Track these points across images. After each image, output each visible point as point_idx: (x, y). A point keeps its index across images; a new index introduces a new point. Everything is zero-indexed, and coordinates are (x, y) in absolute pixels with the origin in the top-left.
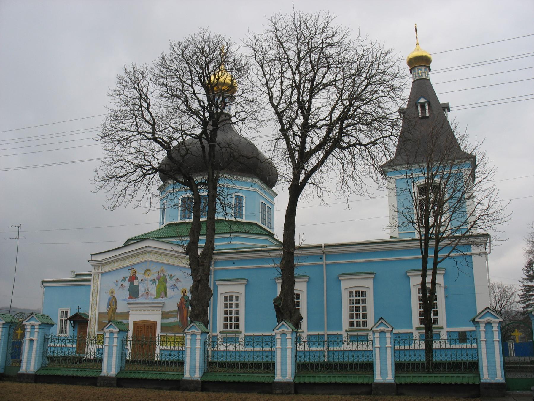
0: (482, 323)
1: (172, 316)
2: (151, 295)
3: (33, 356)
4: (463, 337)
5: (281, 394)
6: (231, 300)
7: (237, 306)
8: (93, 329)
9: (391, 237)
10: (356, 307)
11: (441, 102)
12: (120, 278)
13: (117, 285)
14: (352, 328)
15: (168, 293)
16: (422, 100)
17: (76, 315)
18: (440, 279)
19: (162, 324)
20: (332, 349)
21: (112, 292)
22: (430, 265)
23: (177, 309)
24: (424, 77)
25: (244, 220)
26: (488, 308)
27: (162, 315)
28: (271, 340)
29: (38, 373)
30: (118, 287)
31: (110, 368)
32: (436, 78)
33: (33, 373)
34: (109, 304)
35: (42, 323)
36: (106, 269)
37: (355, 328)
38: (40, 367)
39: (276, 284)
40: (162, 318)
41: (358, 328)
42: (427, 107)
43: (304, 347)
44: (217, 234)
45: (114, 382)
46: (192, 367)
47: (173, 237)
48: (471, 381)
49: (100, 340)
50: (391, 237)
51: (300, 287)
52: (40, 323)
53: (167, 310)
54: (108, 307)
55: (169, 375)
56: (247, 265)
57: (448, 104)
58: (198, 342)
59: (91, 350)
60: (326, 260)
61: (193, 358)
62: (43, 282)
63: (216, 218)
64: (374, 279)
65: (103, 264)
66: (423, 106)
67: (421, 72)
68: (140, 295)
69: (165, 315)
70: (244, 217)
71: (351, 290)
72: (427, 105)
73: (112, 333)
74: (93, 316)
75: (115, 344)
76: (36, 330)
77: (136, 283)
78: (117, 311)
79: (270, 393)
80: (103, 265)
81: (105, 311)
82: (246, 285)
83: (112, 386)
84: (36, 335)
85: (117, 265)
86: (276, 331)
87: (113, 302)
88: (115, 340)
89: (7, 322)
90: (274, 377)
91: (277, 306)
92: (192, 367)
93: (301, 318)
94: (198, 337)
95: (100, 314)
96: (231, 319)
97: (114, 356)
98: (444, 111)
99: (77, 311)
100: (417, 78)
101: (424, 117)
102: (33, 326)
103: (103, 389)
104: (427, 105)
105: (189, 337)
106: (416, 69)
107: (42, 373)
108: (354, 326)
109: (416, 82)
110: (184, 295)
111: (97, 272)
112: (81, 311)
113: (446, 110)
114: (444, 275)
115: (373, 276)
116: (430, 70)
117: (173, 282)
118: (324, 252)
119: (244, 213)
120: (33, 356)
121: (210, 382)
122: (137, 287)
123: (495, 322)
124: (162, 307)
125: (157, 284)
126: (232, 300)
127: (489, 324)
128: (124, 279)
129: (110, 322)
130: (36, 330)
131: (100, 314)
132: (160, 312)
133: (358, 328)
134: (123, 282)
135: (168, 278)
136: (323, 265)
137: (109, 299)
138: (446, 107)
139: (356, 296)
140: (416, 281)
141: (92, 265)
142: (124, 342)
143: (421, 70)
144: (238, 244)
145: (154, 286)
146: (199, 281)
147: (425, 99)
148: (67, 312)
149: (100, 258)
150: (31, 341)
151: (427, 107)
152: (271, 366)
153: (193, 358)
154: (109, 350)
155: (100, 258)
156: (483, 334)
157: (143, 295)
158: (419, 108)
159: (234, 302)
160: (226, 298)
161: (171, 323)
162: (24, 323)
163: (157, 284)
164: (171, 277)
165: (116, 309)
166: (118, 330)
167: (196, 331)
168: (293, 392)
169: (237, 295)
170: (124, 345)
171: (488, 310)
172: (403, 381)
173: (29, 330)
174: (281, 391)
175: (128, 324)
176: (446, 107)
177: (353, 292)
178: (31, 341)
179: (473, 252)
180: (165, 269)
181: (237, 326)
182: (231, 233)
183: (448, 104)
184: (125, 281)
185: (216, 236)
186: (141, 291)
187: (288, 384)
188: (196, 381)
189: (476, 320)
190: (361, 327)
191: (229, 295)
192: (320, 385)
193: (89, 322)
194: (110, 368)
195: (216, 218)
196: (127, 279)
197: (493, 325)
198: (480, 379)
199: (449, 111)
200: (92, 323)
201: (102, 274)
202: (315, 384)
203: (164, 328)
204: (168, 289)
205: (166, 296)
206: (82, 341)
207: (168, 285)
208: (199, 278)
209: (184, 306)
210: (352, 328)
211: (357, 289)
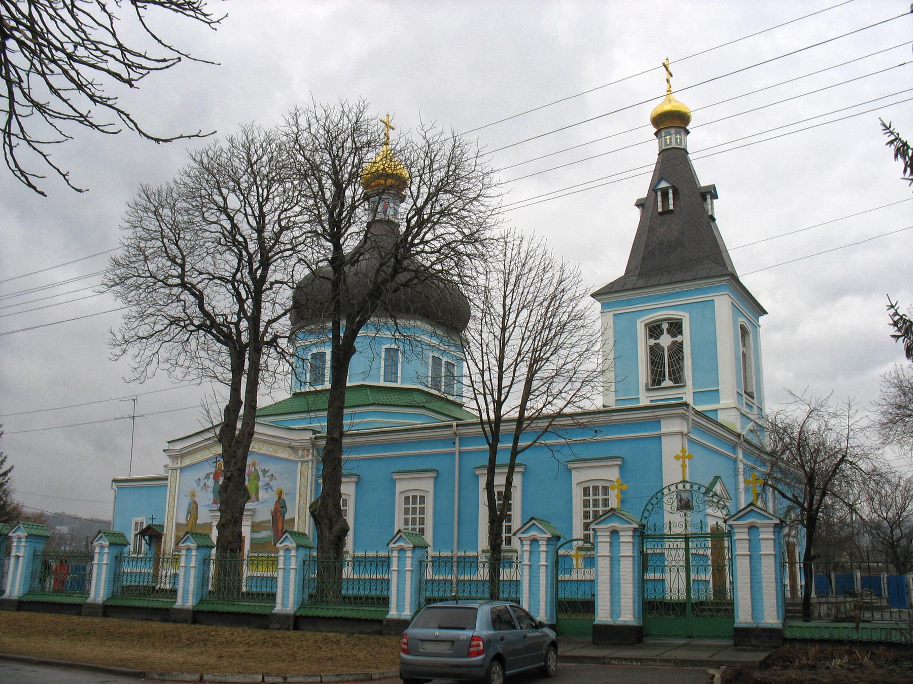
1: (264, 529)
3: (18, 577)
5: (278, 629)
6: (415, 501)
7: (422, 510)
8: (169, 543)
9: (604, 406)
12: (202, 475)
13: (199, 485)
15: (260, 495)
16: (663, 185)
17: (149, 528)
18: (517, 480)
19: (252, 539)
20: (703, 578)
21: (193, 495)
22: (503, 458)
23: (270, 518)
25: (399, 385)
27: (252, 526)
28: (385, 562)
29: (297, 615)
30: (200, 488)
31: (287, 601)
33: (16, 598)
34: (189, 512)
35: (29, 535)
36: (187, 461)
38: (27, 591)
39: (477, 476)
42: (671, 196)
43: (429, 574)
44: (347, 407)
45: (100, 611)
46: (185, 592)
47: (296, 413)
49: (176, 559)
50: (604, 406)
51: (347, 489)
53: (258, 519)
55: (160, 603)
56: (636, 432)
58: (409, 562)
59: (167, 571)
60: (460, 446)
61: (401, 591)
62: (115, 481)
63: (348, 385)
64: (621, 467)
65: (182, 455)
67: (672, 139)
70: (399, 380)
72: (670, 191)
73: (189, 549)
74: (170, 528)
75: (193, 564)
76: (23, 544)
78: (198, 522)
79: (266, 628)
80: (183, 456)
82: (357, 483)
83: (97, 615)
84: (22, 549)
85: (199, 457)
86: (391, 545)
88: (293, 560)
89: (29, 535)
92: (185, 592)
93: (345, 531)
94: (409, 554)
95: (178, 525)
97: (103, 577)
98: (704, 199)
100: (664, 148)
101: (666, 212)
103: (88, 619)
104: (670, 191)
105: (281, 553)
107: (205, 607)
110: (280, 498)
111: (175, 466)
112: (155, 522)
113: (709, 197)
114: (523, 474)
115: (620, 463)
117: (267, 479)
118: (455, 433)
119: (399, 375)
120: (18, 577)
121: (203, 612)
124: (253, 516)
126: (414, 502)
128: (207, 476)
129: (187, 533)
130: (23, 544)
131: (178, 525)
132: (250, 523)
134: (206, 481)
135: (260, 474)
136: (454, 453)
137: (189, 505)
140: (483, 482)
141: (170, 456)
142: (205, 562)
144: (374, 422)
147: (668, 182)
149: (179, 446)
150: (18, 557)
151: (671, 196)
152: (272, 597)
153: (401, 591)
155: (179, 446)
156: (526, 555)
158: (659, 198)
159: (601, 497)
160: (586, 491)
161: (262, 538)
162: (10, 534)
164: (265, 472)
165: (196, 518)
166: (294, 545)
168: (291, 628)
170: (423, 569)
173: (15, 544)
174: (278, 626)
176: (711, 193)
178: (18, 557)
179: (664, 430)
180: (257, 462)
182: (309, 412)
183: (714, 187)
185: (346, 411)
187: (286, 617)
188: (187, 611)
191: (591, 485)
192: (324, 618)
194: (287, 601)
195: (348, 385)
196: (211, 476)
197: (540, 542)
200: (168, 538)
201: (181, 469)
202: (318, 617)
203: (254, 544)
205: (258, 500)
206: (157, 560)
207: (261, 484)
209: (279, 514)
211: (414, 494)
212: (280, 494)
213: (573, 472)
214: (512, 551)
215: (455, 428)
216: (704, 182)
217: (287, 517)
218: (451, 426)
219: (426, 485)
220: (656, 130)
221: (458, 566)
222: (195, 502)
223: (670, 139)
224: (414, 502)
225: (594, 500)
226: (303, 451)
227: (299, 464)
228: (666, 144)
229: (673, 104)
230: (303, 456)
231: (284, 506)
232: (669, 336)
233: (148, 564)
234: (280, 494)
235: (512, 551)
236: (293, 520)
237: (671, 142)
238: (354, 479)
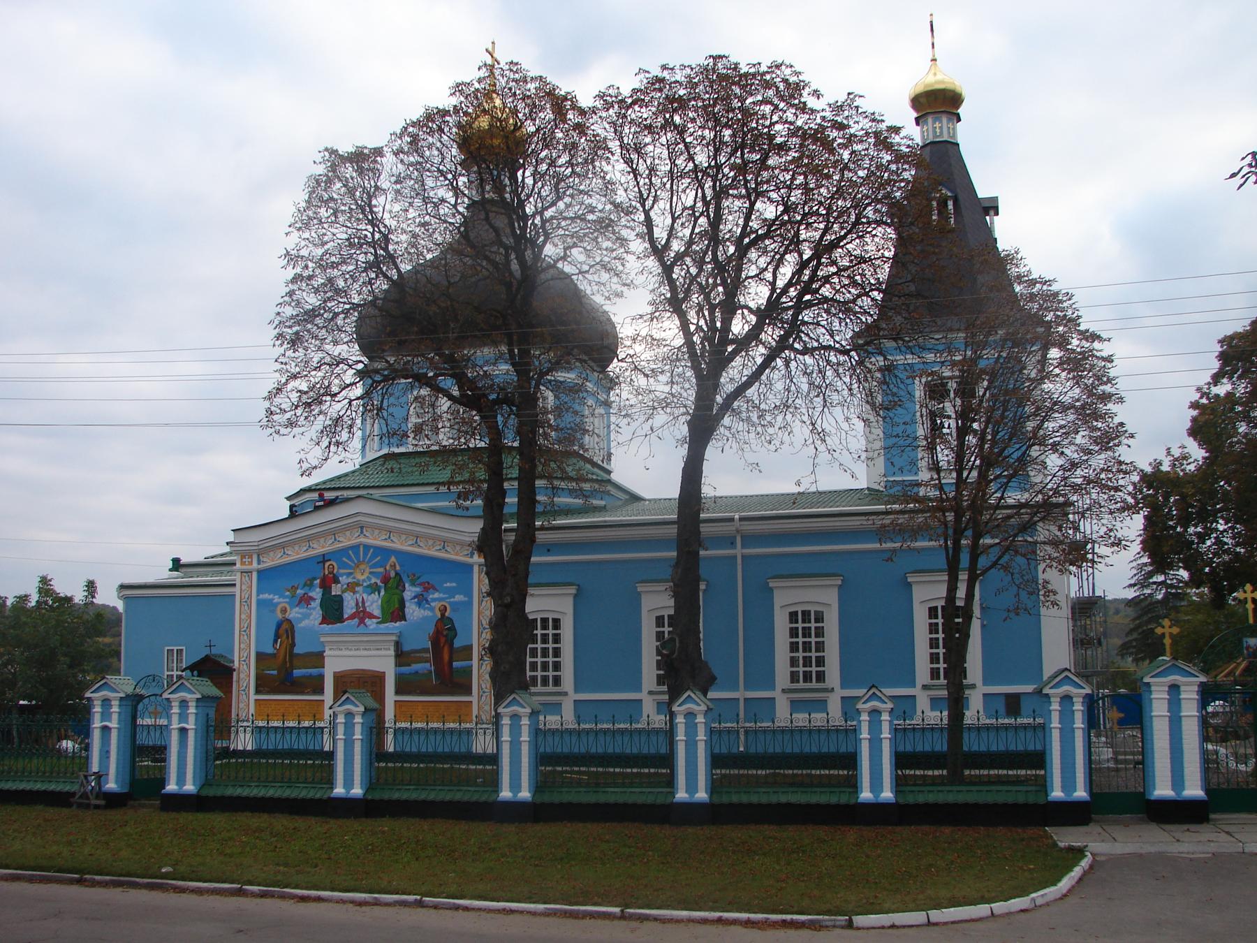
0: (1055, 695)
2: (371, 616)
4: (1013, 704)
11: (981, 194)
14: (795, 686)
24: (945, 138)
26: (1066, 669)
32: (971, 136)
35: (203, 697)
37: (801, 685)
40: (399, 664)
41: (808, 685)
48: (1031, 799)
52: (199, 696)
54: (275, 641)
57: (995, 199)
60: (743, 547)
62: (123, 587)
66: (943, 204)
67: (938, 128)
68: (346, 616)
69: (402, 657)
71: (793, 609)
77: (336, 590)
81: (269, 650)
87: (285, 630)
90: (673, 794)
91: (667, 656)
95: (260, 657)
96: (545, 667)
99: (206, 652)
102: (184, 704)
106: (930, 120)
108: (798, 681)
109: (928, 148)
110: (443, 615)
116: (959, 120)
122: (339, 600)
123: (1078, 695)
125: (382, 593)
126: (545, 627)
127: (1067, 698)
133: (808, 685)
138: (991, 207)
139: (804, 621)
143: (941, 122)
145: (375, 596)
146: (508, 606)
148: (180, 652)
150: (183, 731)
154: (345, 747)
157: (352, 617)
159: (551, 632)
160: (793, 617)
163: (382, 593)
165: (293, 645)
166: (362, 709)
167: (521, 710)
169: (556, 616)
171: (1066, 673)
172: (911, 799)
175: (322, 677)
176: (991, 207)
177: (796, 613)
181: (557, 681)
183: (995, 199)
186: (349, 608)
189: (1045, 691)
190: (814, 685)
191: (799, 609)
193: (235, 674)
198: (1047, 795)
199: (997, 214)
200: (242, 676)
204: (407, 604)
208: (508, 600)
209: (443, 640)
210: (795, 686)
211: (806, 608)
213: (914, 588)
214: (560, 694)
215: (737, 523)
216: (982, 192)
217: (458, 643)
218: (732, 520)
219: (825, 598)
220: (915, 115)
223: (941, 128)
224: (545, 627)
228: (935, 136)
229: (940, 77)
235: (560, 694)
237: (941, 132)
238: (573, 590)
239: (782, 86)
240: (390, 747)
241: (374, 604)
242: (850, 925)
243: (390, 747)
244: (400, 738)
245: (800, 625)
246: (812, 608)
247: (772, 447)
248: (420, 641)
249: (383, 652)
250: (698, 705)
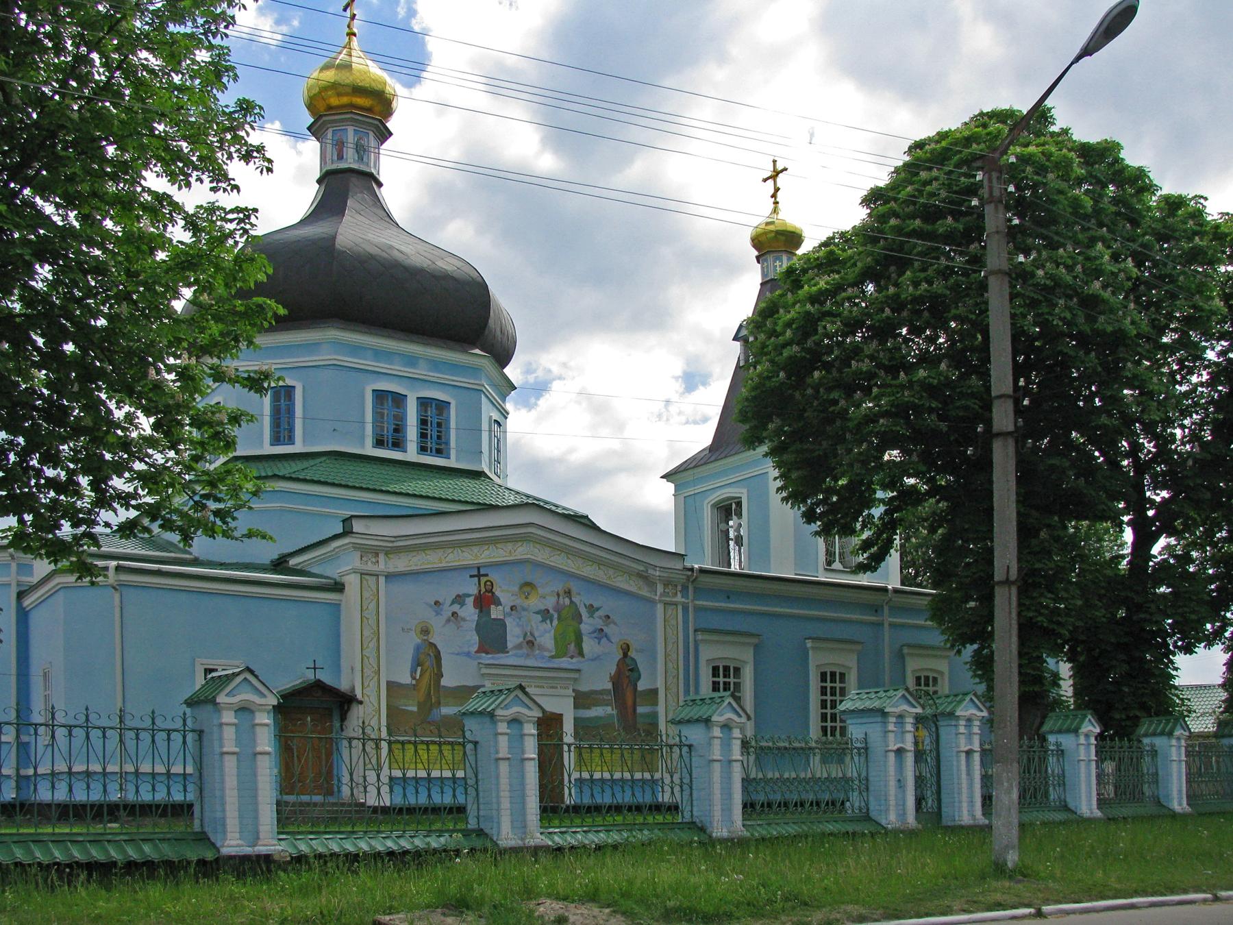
2: (541, 648)
10: (725, 683)
21: (425, 631)
23: (609, 686)
25: (452, 463)
68: (510, 645)
69: (582, 700)
70: (453, 453)
77: (495, 612)
85: (432, 560)
105: (228, 717)
110: (625, 655)
117: (599, 623)
122: (501, 624)
125: (555, 622)
126: (927, 685)
134: (456, 608)
145: (547, 626)
157: (519, 647)
161: (597, 718)
163: (555, 622)
164: (592, 609)
180: (574, 590)
184: (462, 604)
186: (513, 636)
191: (922, 674)
196: (470, 601)
204: (585, 638)
205: (581, 654)
211: (926, 674)
212: (626, 649)
217: (642, 686)
220: (756, 253)
221: (391, 791)
222: (433, 645)
225: (841, 688)
226: (666, 585)
227: (660, 607)
230: (664, 594)
231: (634, 670)
232: (524, 411)
233: (607, 756)
234: (626, 649)
236: (654, 692)
239: (907, 285)
240: (570, 797)
241: (546, 636)
242: (1039, 914)
243: (570, 797)
244: (398, 753)
245: (829, 685)
246: (931, 675)
247: (561, 593)
248: (600, 680)
249: (563, 692)
250: (263, 695)
